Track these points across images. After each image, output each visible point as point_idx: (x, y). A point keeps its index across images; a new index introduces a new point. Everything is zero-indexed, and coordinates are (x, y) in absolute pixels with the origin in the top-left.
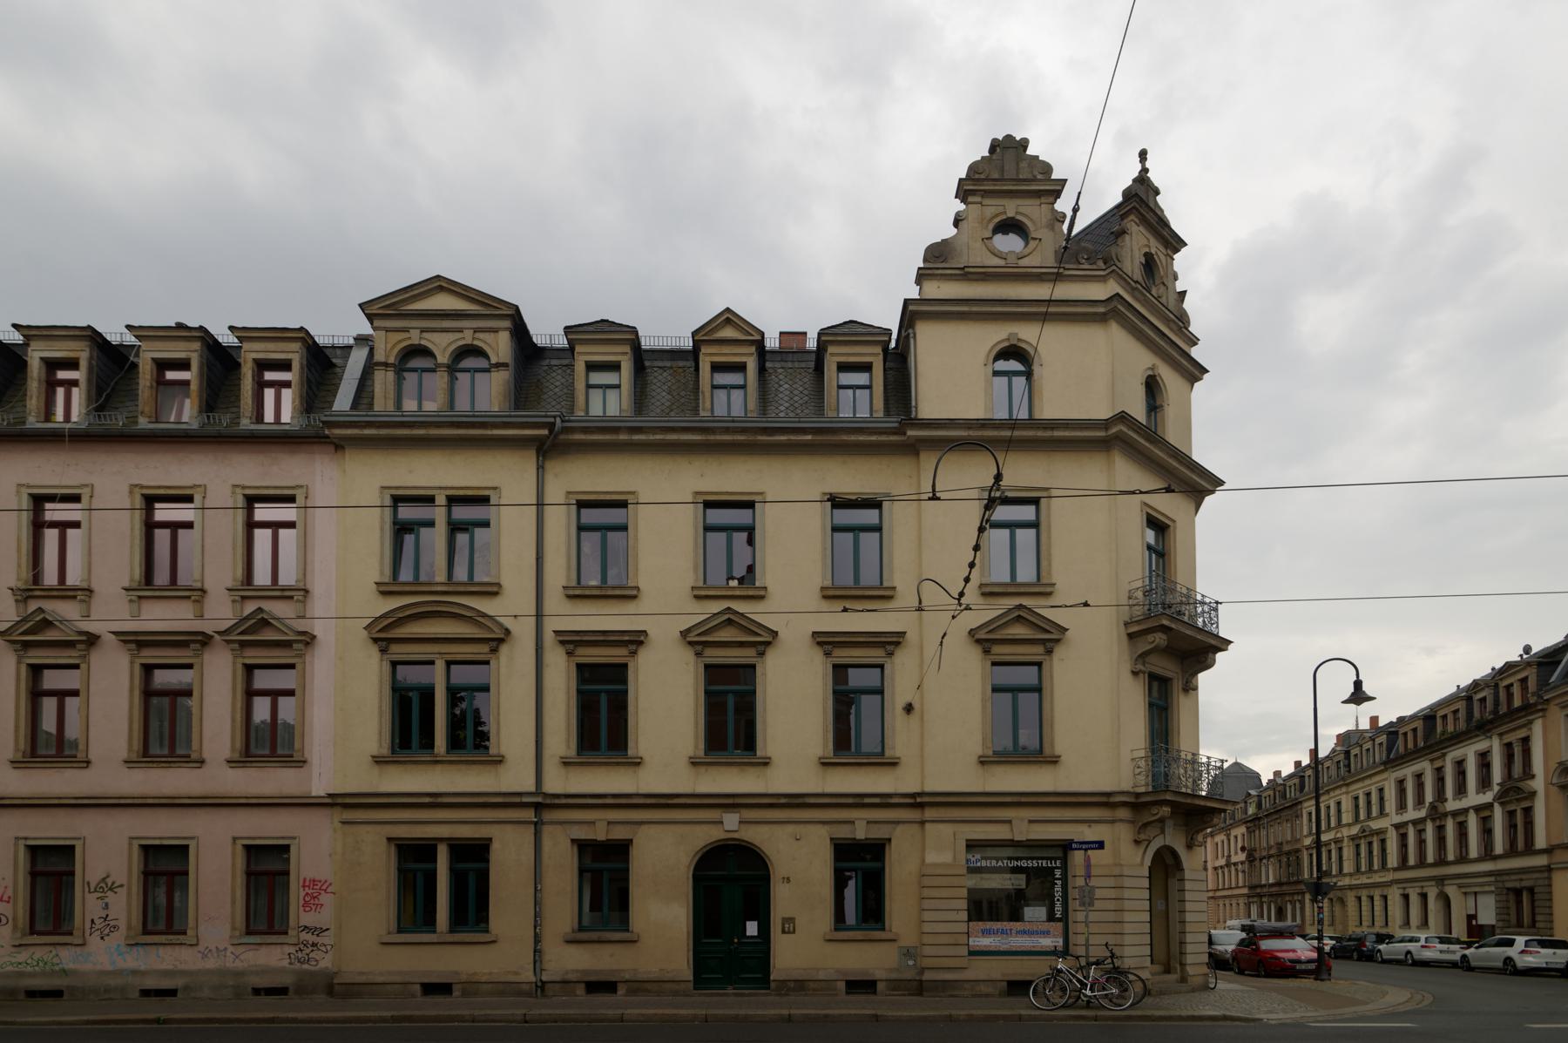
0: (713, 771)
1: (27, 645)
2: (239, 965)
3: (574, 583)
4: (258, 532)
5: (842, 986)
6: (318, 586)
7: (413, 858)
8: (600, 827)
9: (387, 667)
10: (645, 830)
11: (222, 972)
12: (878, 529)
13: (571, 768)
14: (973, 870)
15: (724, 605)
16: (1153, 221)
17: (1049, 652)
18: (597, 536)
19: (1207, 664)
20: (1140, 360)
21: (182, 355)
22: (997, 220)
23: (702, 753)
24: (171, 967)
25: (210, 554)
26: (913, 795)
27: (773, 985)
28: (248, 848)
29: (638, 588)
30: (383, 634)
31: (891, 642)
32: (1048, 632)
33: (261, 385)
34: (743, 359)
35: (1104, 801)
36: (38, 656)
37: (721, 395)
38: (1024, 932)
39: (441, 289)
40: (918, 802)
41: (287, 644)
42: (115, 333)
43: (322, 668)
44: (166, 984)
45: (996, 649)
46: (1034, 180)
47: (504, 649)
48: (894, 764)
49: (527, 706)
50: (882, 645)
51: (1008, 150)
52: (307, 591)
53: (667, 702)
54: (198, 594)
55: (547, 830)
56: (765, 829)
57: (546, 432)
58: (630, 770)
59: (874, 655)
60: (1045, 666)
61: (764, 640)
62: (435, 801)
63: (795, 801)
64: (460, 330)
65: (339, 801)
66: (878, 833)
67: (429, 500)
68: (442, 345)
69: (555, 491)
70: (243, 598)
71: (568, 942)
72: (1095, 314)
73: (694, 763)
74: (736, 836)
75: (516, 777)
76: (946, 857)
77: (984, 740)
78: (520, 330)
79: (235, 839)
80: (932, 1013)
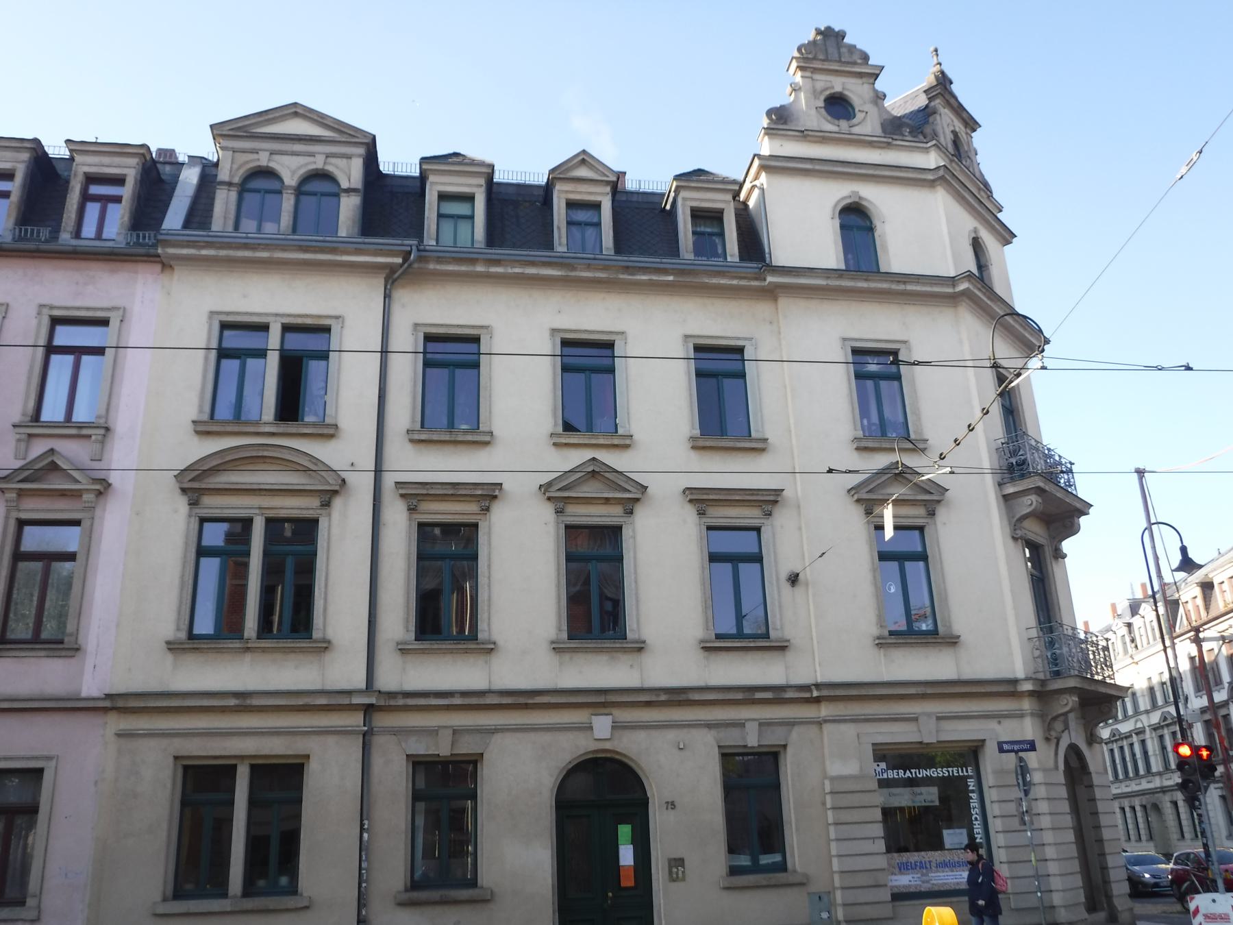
0: (580, 658)
1: (21, 493)
3: (206, 417)
4: (55, 359)
6: (121, 424)
7: (203, 783)
8: (439, 736)
9: (195, 525)
10: (796, 734)
13: (409, 658)
14: (884, 784)
15: (588, 454)
16: (956, 105)
17: (326, 504)
18: (444, 372)
19: (1072, 530)
20: (967, 223)
21: (7, 166)
22: (828, 93)
23: (565, 635)
26: (806, 688)
29: (336, 426)
30: (195, 483)
31: (768, 501)
33: (86, 198)
34: (598, 198)
36: (34, 508)
37: (447, 226)
39: (296, 114)
40: (813, 694)
41: (76, 494)
42: (56, 148)
43: (114, 525)
46: (855, 63)
47: (337, 503)
48: (782, 648)
49: (360, 573)
50: (759, 504)
51: (831, 37)
52: (107, 429)
53: (521, 572)
55: (379, 741)
56: (641, 735)
57: (400, 260)
58: (776, 654)
59: (747, 515)
60: (926, 531)
61: (631, 496)
62: (243, 702)
63: (678, 697)
64: (312, 155)
65: (120, 704)
66: (773, 738)
67: (264, 328)
68: (290, 168)
70: (30, 436)
71: (402, 904)
72: (925, 180)
74: (608, 746)
75: (344, 670)
76: (850, 768)
78: (371, 158)
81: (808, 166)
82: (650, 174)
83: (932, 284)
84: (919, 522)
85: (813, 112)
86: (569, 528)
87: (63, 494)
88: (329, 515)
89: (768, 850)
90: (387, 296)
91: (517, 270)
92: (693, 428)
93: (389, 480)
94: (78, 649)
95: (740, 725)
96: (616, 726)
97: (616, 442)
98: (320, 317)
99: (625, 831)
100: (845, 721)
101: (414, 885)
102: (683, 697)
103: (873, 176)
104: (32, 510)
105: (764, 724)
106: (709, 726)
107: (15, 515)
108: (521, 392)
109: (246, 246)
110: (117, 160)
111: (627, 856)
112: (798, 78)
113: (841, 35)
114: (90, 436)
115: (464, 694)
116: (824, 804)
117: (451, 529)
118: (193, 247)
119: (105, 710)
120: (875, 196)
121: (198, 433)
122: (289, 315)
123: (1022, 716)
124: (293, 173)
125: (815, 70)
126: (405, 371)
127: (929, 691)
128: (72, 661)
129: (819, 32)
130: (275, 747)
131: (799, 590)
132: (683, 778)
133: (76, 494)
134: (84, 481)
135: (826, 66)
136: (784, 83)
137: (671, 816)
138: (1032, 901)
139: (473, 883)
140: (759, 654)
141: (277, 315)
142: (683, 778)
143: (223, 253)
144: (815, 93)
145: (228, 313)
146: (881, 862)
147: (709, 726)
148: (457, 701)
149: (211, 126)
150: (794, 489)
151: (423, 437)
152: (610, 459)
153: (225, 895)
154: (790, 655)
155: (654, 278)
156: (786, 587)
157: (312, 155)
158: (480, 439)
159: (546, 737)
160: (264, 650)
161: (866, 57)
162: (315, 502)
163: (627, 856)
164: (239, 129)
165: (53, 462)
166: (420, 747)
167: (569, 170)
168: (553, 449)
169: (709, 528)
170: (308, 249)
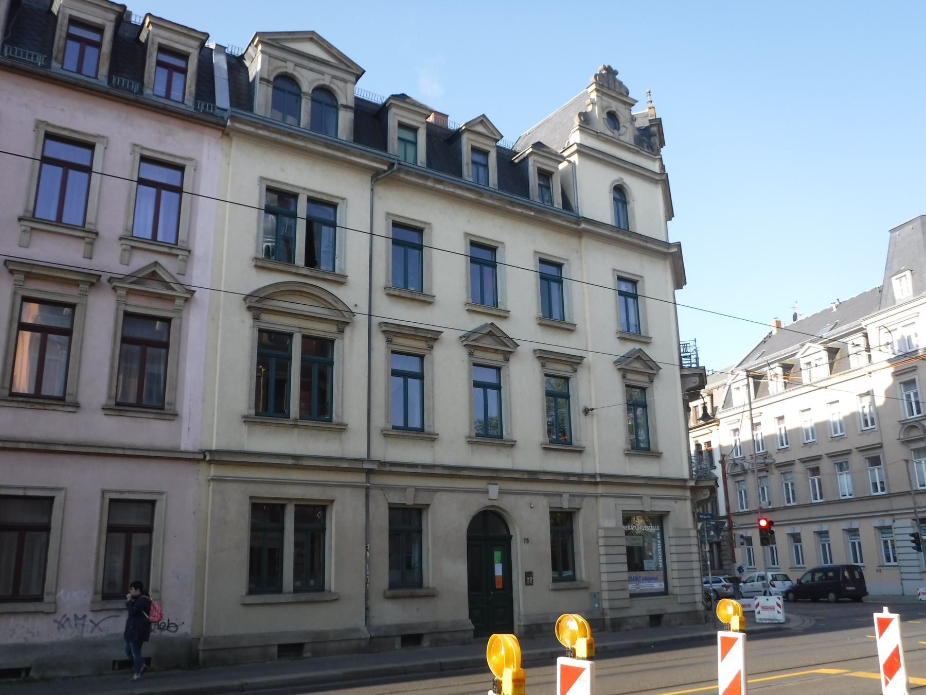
0: (482, 448)
1: (130, 292)
2: (97, 634)
5: (275, 650)
7: (266, 515)
8: (406, 492)
11: (80, 644)
15: (489, 320)
21: (98, 21)
23: (253, 412)
24: (21, 641)
25: (113, 202)
26: (594, 476)
28: (112, 501)
31: (575, 362)
32: (506, 345)
34: (489, 149)
38: (646, 579)
39: (311, 39)
40: (593, 480)
41: (172, 299)
44: (18, 662)
45: (478, 354)
46: (622, 94)
47: (347, 330)
54: (88, 235)
55: (373, 493)
57: (386, 168)
58: (575, 455)
59: (417, 345)
60: (502, 372)
62: (297, 462)
64: (322, 73)
68: (308, 81)
69: (381, 209)
70: (133, 247)
71: (387, 598)
73: (247, 420)
74: (495, 503)
75: (354, 446)
79: (104, 492)
80: (396, 665)
81: (601, 156)
83: (659, 246)
84: (645, 385)
85: (602, 120)
87: (159, 297)
88: (343, 339)
89: (566, 568)
90: (372, 190)
91: (451, 190)
93: (375, 321)
94: (177, 415)
95: (560, 495)
96: (502, 492)
97: (638, 339)
98: (332, 196)
99: (497, 555)
101: (392, 586)
102: (535, 477)
103: (605, 161)
104: (137, 306)
105: (572, 496)
106: (546, 494)
107: (123, 307)
108: (447, 273)
109: (289, 135)
110: (183, 39)
111: (498, 570)
112: (594, 95)
113: (616, 73)
114: (177, 256)
115: (425, 466)
116: (597, 543)
118: (253, 126)
119: (198, 461)
120: (634, 185)
121: (256, 266)
122: (312, 191)
123: (685, 499)
124: (310, 83)
125: (604, 93)
126: (383, 247)
128: (173, 423)
129: (605, 68)
130: (314, 494)
131: (588, 417)
133: (172, 299)
134: (179, 290)
135: (609, 92)
136: (589, 96)
137: (526, 546)
138: (687, 599)
139: (420, 585)
140: (569, 454)
141: (305, 189)
142: (530, 523)
143: (274, 136)
144: (602, 109)
145: (272, 181)
146: (625, 576)
147: (546, 494)
148: (419, 470)
149: (364, 72)
150: (590, 358)
151: (396, 293)
152: (498, 323)
153: (280, 591)
154: (584, 456)
155: (524, 211)
156: (582, 414)
157: (322, 73)
158: (427, 301)
159: (464, 496)
160: (306, 427)
161: (628, 93)
163: (498, 570)
164: (273, 40)
165: (154, 273)
166: (396, 498)
167: (474, 125)
168: (466, 313)
169: (393, 352)
170: (316, 142)
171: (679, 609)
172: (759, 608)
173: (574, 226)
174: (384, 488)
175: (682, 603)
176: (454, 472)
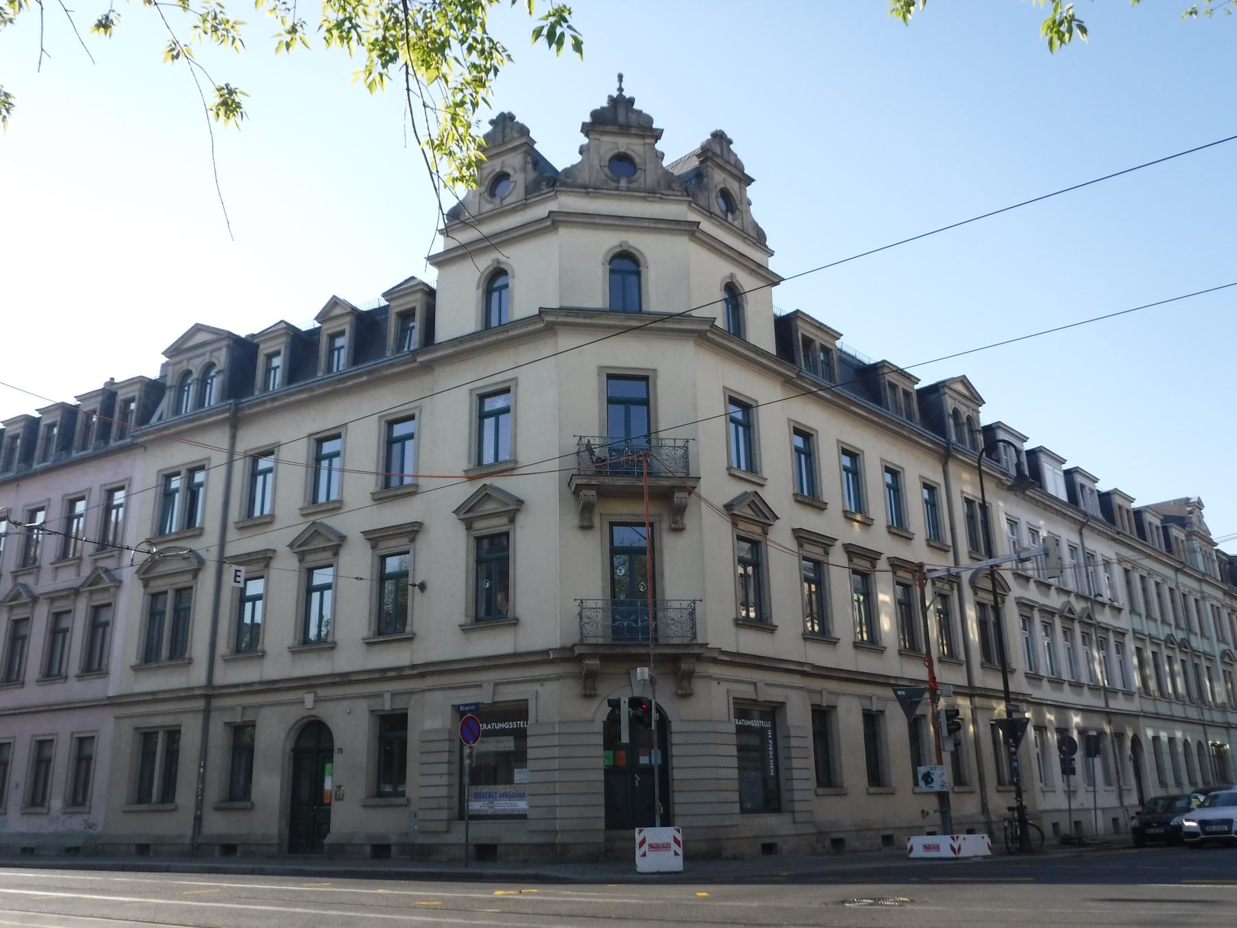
1: (91, 592)
7: (147, 737)
10: (266, 712)
12: (646, 402)
17: (512, 520)
27: (326, 848)
32: (330, 540)
35: (540, 658)
47: (201, 575)
50: (66, 597)
55: (214, 715)
56: (329, 705)
59: (400, 543)
61: (514, 508)
63: (344, 679)
64: (204, 354)
74: (313, 713)
75: (197, 675)
77: (466, 609)
82: (367, 298)
83: (526, 325)
84: (504, 529)
86: (479, 540)
92: (469, 462)
95: (379, 695)
96: (317, 701)
100: (439, 689)
115: (245, 685)
117: (492, 537)
120: (640, 242)
127: (487, 664)
129: (492, 122)
130: (169, 721)
132: (352, 731)
162: (189, 577)
171: (524, 839)
172: (645, 847)
173: (414, 365)
174: (222, 709)
175: (532, 831)
176: (270, 686)
